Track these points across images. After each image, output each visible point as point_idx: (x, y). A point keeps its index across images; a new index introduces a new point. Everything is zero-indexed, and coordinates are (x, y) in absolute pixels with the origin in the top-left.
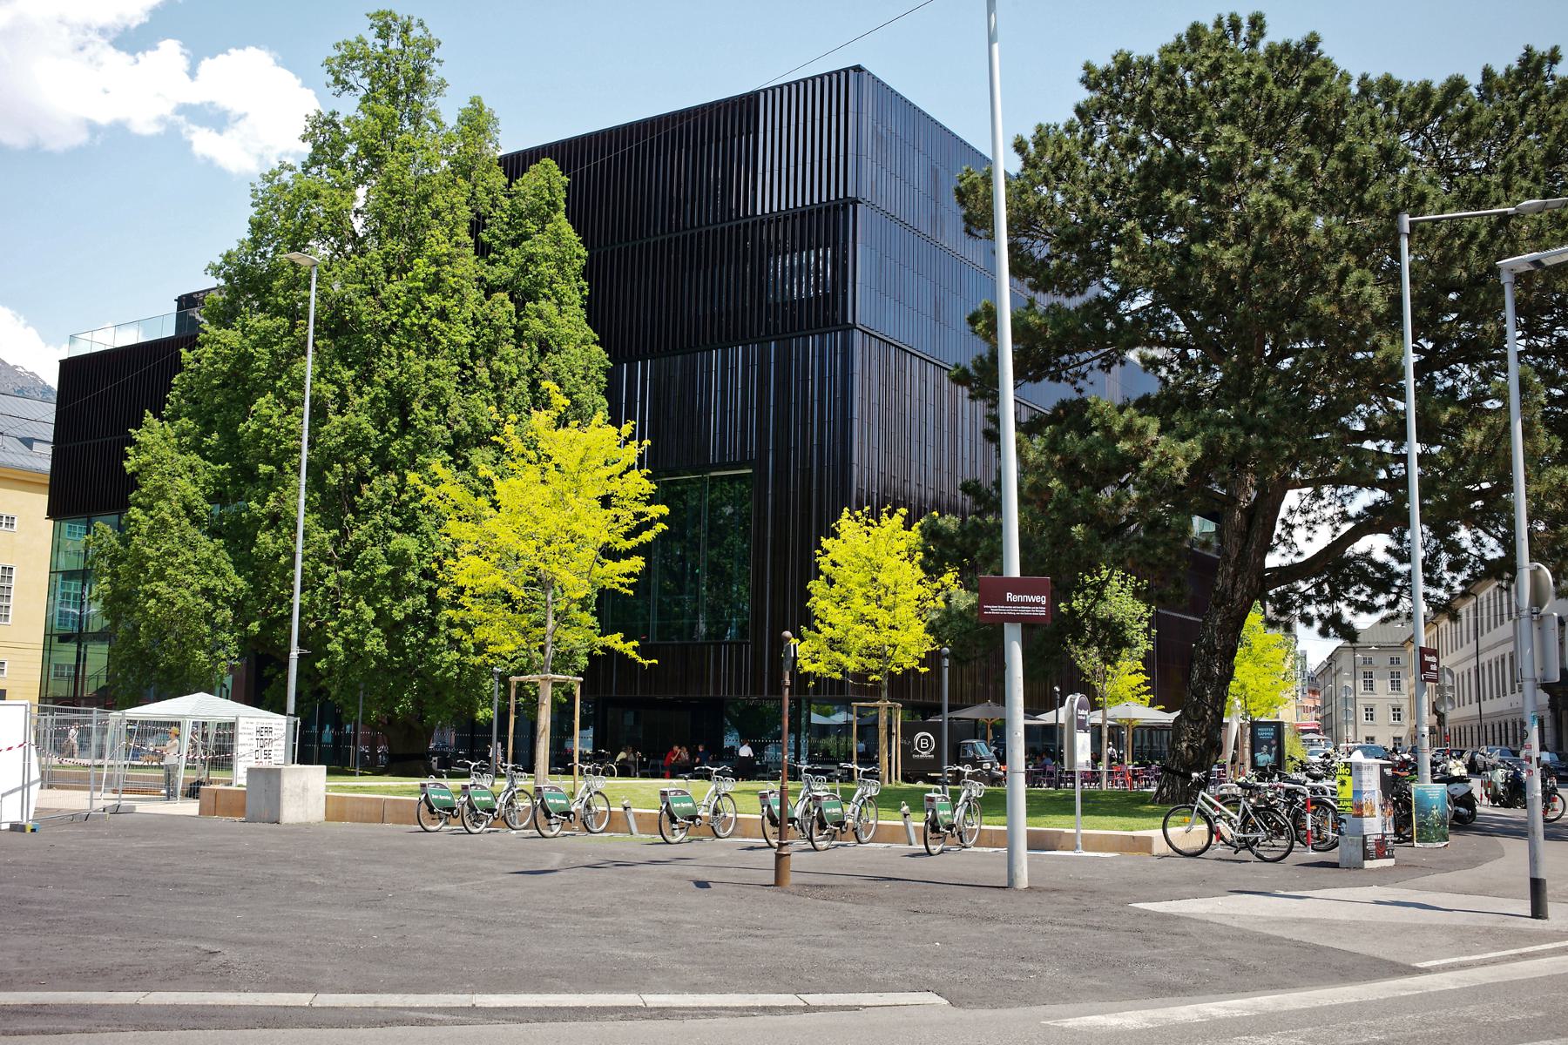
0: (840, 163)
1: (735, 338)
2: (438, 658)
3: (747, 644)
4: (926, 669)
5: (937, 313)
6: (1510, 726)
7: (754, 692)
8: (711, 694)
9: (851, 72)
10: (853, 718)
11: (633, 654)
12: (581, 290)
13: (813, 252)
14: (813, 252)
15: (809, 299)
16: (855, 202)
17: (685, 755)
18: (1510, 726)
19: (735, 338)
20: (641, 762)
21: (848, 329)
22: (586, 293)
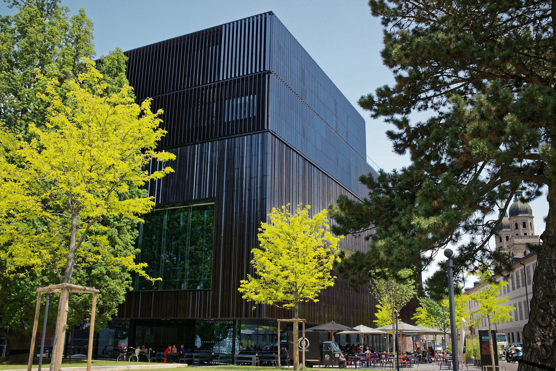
0: (262, 55)
1: (208, 138)
2: (35, 293)
4: (318, 300)
5: (304, 133)
6: (515, 334)
7: (213, 316)
9: (268, 14)
11: (143, 273)
13: (247, 97)
14: (247, 97)
15: (245, 119)
16: (269, 72)
17: (175, 350)
18: (515, 334)
19: (208, 138)
20: (152, 353)
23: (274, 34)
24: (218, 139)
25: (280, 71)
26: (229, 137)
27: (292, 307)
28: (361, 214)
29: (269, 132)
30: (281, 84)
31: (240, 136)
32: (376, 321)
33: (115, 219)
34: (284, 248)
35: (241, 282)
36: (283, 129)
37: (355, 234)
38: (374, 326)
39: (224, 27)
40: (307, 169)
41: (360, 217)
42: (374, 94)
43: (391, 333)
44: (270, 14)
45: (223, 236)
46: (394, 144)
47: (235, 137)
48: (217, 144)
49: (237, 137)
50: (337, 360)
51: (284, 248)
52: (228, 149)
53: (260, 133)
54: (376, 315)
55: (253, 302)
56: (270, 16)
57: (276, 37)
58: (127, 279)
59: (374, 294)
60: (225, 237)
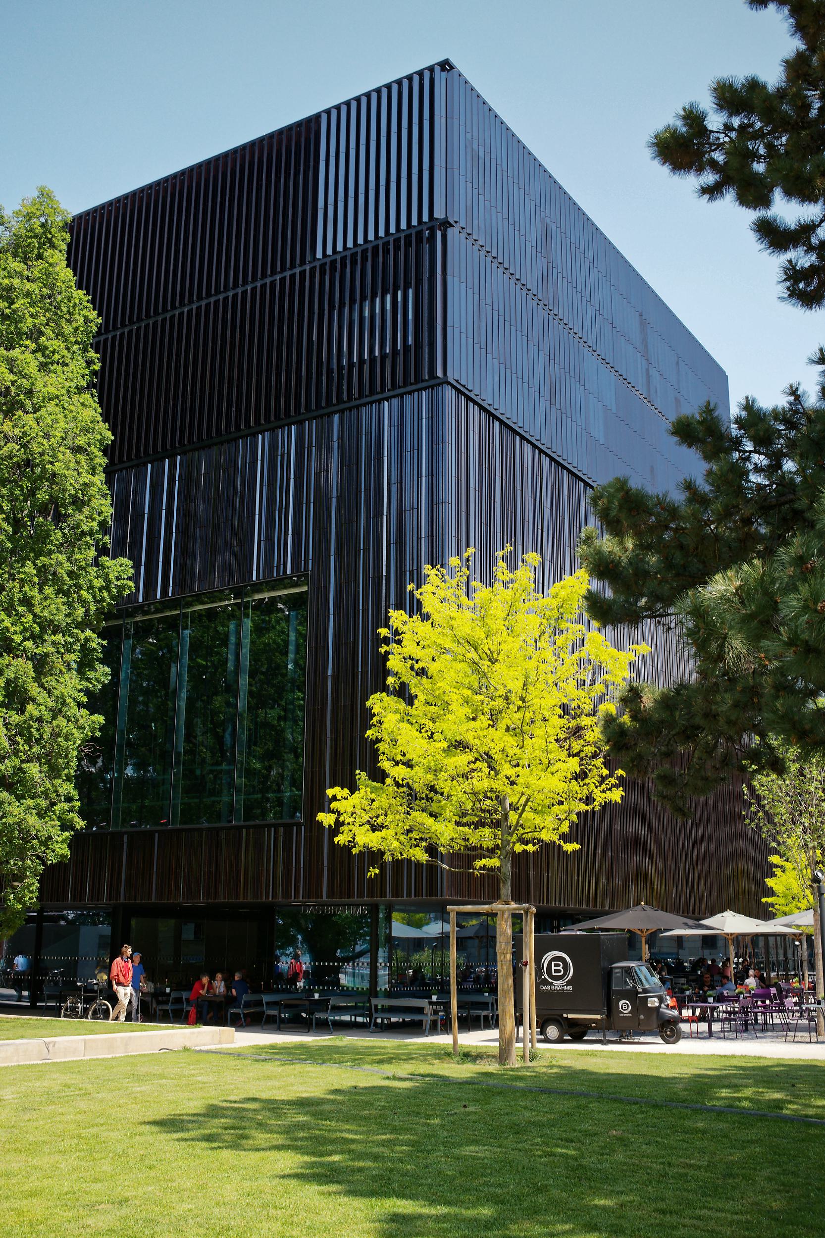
3: (298, 825)
4: (576, 846)
7: (308, 895)
8: (264, 899)
9: (437, 68)
10: (450, 928)
12: (89, 363)
13: (389, 298)
14: (389, 298)
16: (446, 224)
17: (220, 986)
21: (436, 384)
22: (97, 367)
23: (456, 121)
24: (315, 414)
25: (476, 222)
26: (342, 406)
27: (492, 869)
28: (681, 547)
29: (449, 383)
30: (482, 257)
31: (371, 403)
32: (770, 900)
33: (28, 635)
34: (458, 685)
35: (330, 792)
36: (490, 380)
37: (664, 620)
38: (765, 913)
39: (324, 118)
40: (566, 493)
41: (678, 558)
42: (706, 103)
43: (811, 931)
44: (443, 69)
45: (333, 676)
46: (786, 271)
47: (358, 407)
48: (312, 428)
49: (365, 405)
50: (655, 1016)
51: (458, 685)
52: (341, 438)
53: (425, 389)
54: (770, 882)
55: (374, 856)
56: (444, 74)
57: (462, 129)
58: (69, 799)
59: (757, 825)
60: (336, 677)
